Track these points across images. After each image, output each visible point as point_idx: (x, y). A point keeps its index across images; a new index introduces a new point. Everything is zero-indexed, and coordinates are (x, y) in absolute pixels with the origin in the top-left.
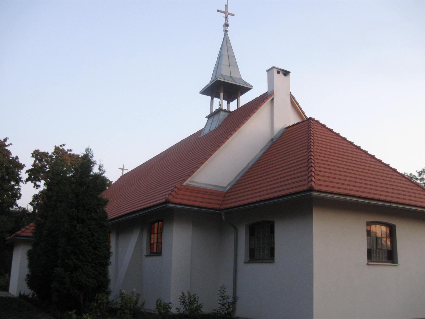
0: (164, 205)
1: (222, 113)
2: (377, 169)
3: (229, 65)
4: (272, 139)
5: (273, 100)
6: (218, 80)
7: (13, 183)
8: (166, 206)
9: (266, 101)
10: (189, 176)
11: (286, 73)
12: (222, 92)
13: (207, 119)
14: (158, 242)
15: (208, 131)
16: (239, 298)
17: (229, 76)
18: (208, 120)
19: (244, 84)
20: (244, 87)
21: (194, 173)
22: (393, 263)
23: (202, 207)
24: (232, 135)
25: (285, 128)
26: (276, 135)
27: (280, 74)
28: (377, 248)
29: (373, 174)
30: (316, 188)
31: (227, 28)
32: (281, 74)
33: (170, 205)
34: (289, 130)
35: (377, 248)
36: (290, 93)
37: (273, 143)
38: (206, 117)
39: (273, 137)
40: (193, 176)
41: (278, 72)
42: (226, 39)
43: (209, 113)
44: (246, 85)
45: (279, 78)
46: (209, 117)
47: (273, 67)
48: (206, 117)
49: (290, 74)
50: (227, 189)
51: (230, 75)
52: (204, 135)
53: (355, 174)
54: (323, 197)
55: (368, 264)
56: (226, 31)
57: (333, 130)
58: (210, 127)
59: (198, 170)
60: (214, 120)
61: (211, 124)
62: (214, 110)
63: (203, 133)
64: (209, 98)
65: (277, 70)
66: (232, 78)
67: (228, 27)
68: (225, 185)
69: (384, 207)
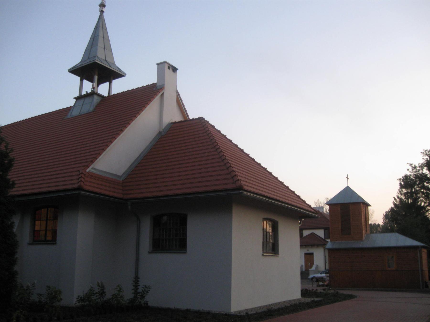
0: (78, 192)
1: (96, 97)
2: (93, 151)
3: (105, 48)
4: (160, 133)
5: (163, 94)
6: (96, 62)
7: (400, 205)
8: (80, 193)
9: (159, 94)
10: (92, 162)
11: (175, 70)
12: (96, 75)
13: (75, 100)
14: (48, 229)
15: (79, 113)
16: (151, 287)
17: (104, 60)
18: (76, 101)
19: (118, 69)
20: (117, 73)
21: (96, 159)
22: (275, 254)
23: (107, 196)
24: (130, 124)
25: (172, 123)
26: (165, 128)
27: (170, 69)
28: (266, 241)
29: (60, 164)
30: (245, 187)
31: (104, 9)
32: (171, 70)
33: (82, 192)
34: (174, 126)
35: (266, 241)
36: (177, 89)
37: (162, 136)
38: (75, 98)
39: (162, 130)
40: (95, 163)
41: (169, 68)
42: (101, 18)
43: (77, 95)
44: (121, 72)
45: (168, 72)
46: (77, 98)
47: (165, 62)
48: (75, 98)
49: (178, 71)
50: (122, 178)
51: (105, 59)
52: (72, 116)
53: (59, 152)
54: (249, 195)
55: (263, 255)
56: (102, 12)
57: (221, 132)
58: (81, 110)
59: (100, 157)
60: (84, 103)
61: (81, 106)
62: (84, 93)
63: (71, 114)
64: (78, 78)
65: (168, 65)
66: (107, 62)
67: (104, 8)
68: (120, 174)
69: (277, 206)
